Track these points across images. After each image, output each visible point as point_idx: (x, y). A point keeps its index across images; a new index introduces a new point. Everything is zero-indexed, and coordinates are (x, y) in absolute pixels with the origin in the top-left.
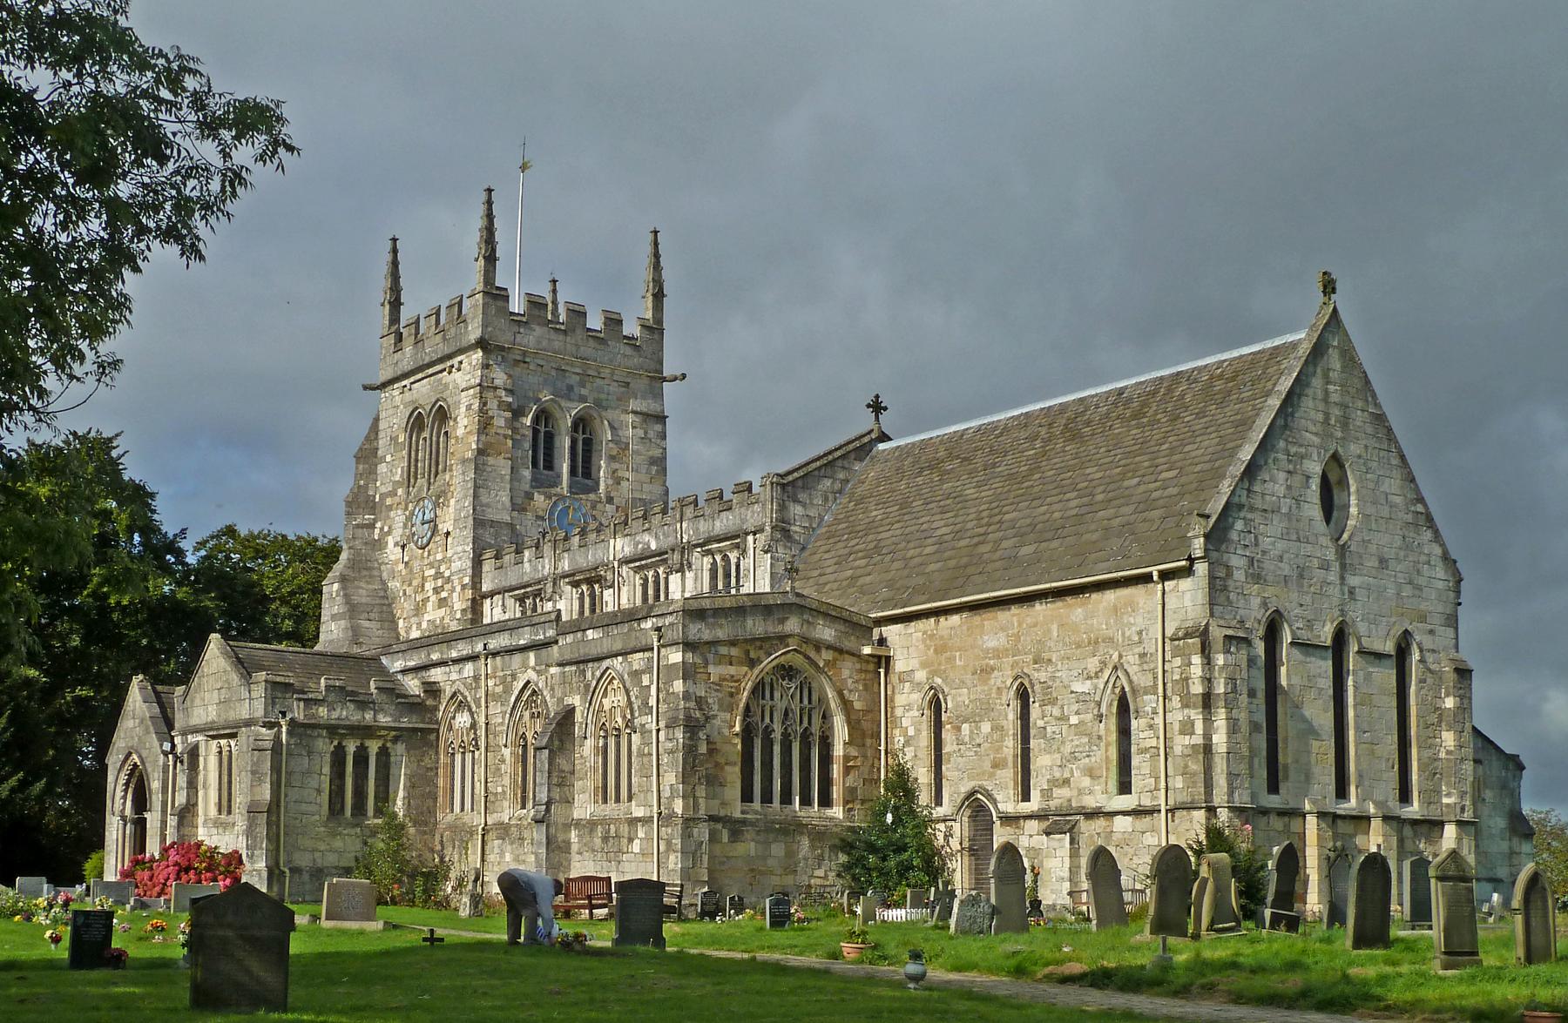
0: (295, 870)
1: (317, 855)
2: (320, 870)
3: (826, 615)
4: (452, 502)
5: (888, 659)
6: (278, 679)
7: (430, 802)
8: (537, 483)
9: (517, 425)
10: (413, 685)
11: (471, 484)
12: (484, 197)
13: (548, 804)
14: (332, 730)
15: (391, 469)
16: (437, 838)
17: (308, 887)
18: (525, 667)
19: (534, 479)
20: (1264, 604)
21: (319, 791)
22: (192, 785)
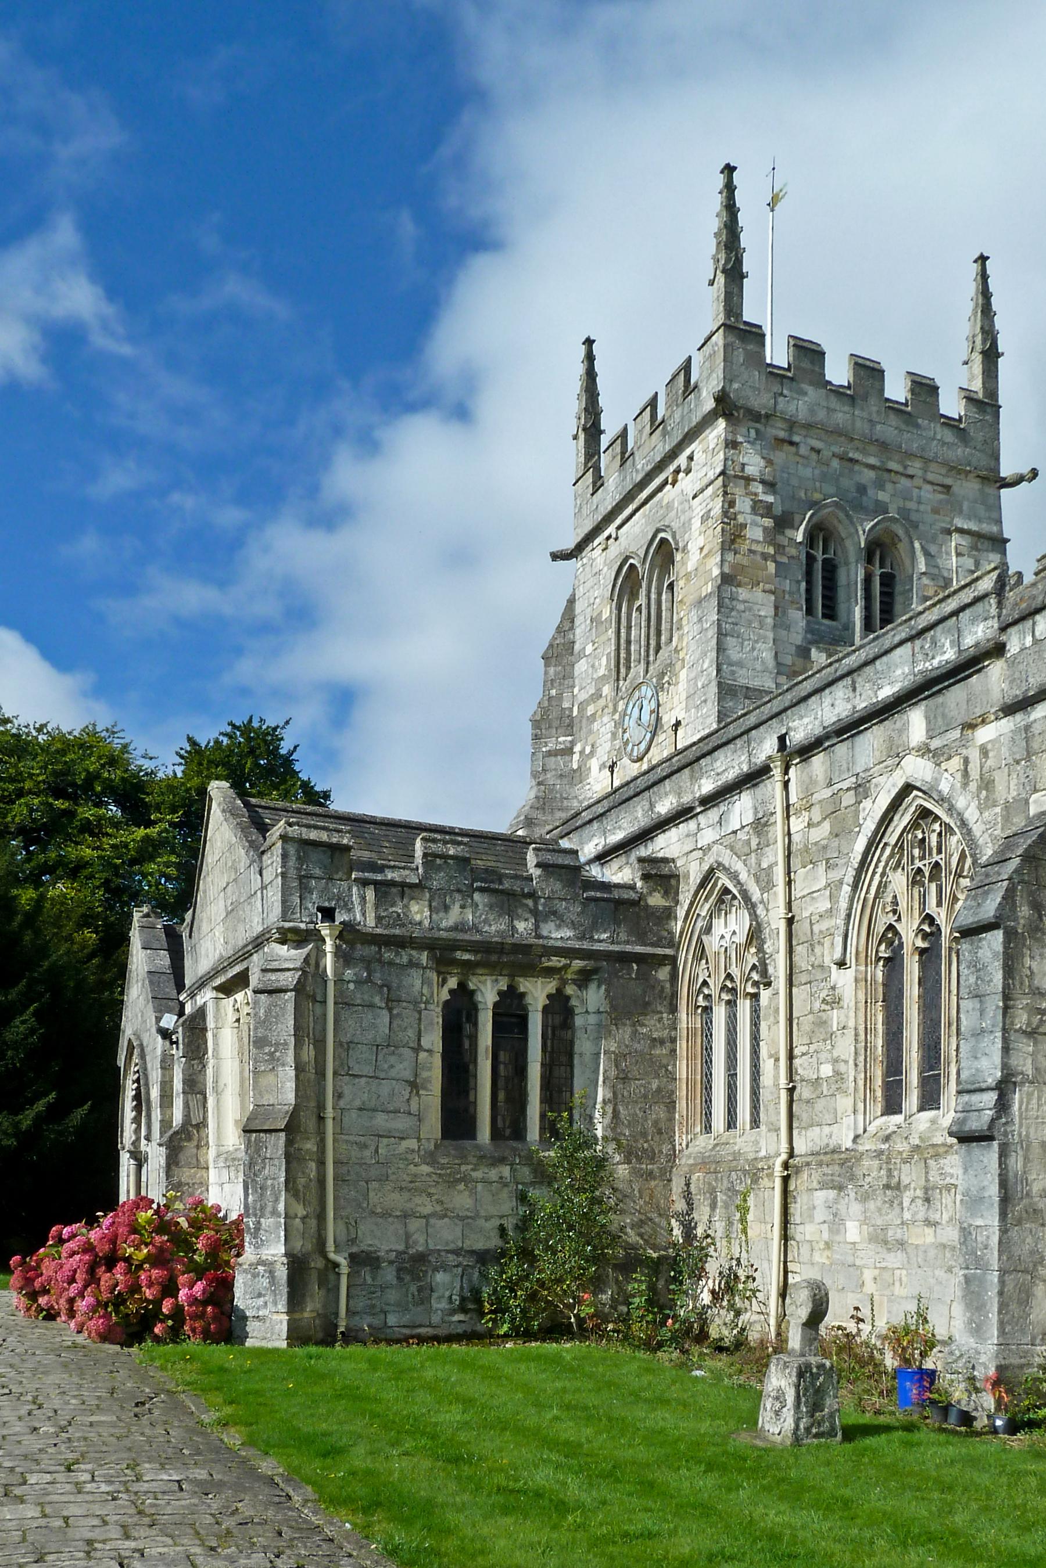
0: (362, 1260)
1: (414, 1225)
2: (421, 1258)
4: (683, 675)
6: (313, 835)
7: (660, 1112)
8: (816, 638)
9: (782, 540)
10: (621, 873)
11: (712, 632)
12: (720, 180)
13: (1005, 1087)
14: (443, 953)
15: (593, 660)
16: (677, 1186)
17: (392, 1296)
18: (896, 754)
19: (809, 630)
21: (415, 1086)
22: (194, 1086)
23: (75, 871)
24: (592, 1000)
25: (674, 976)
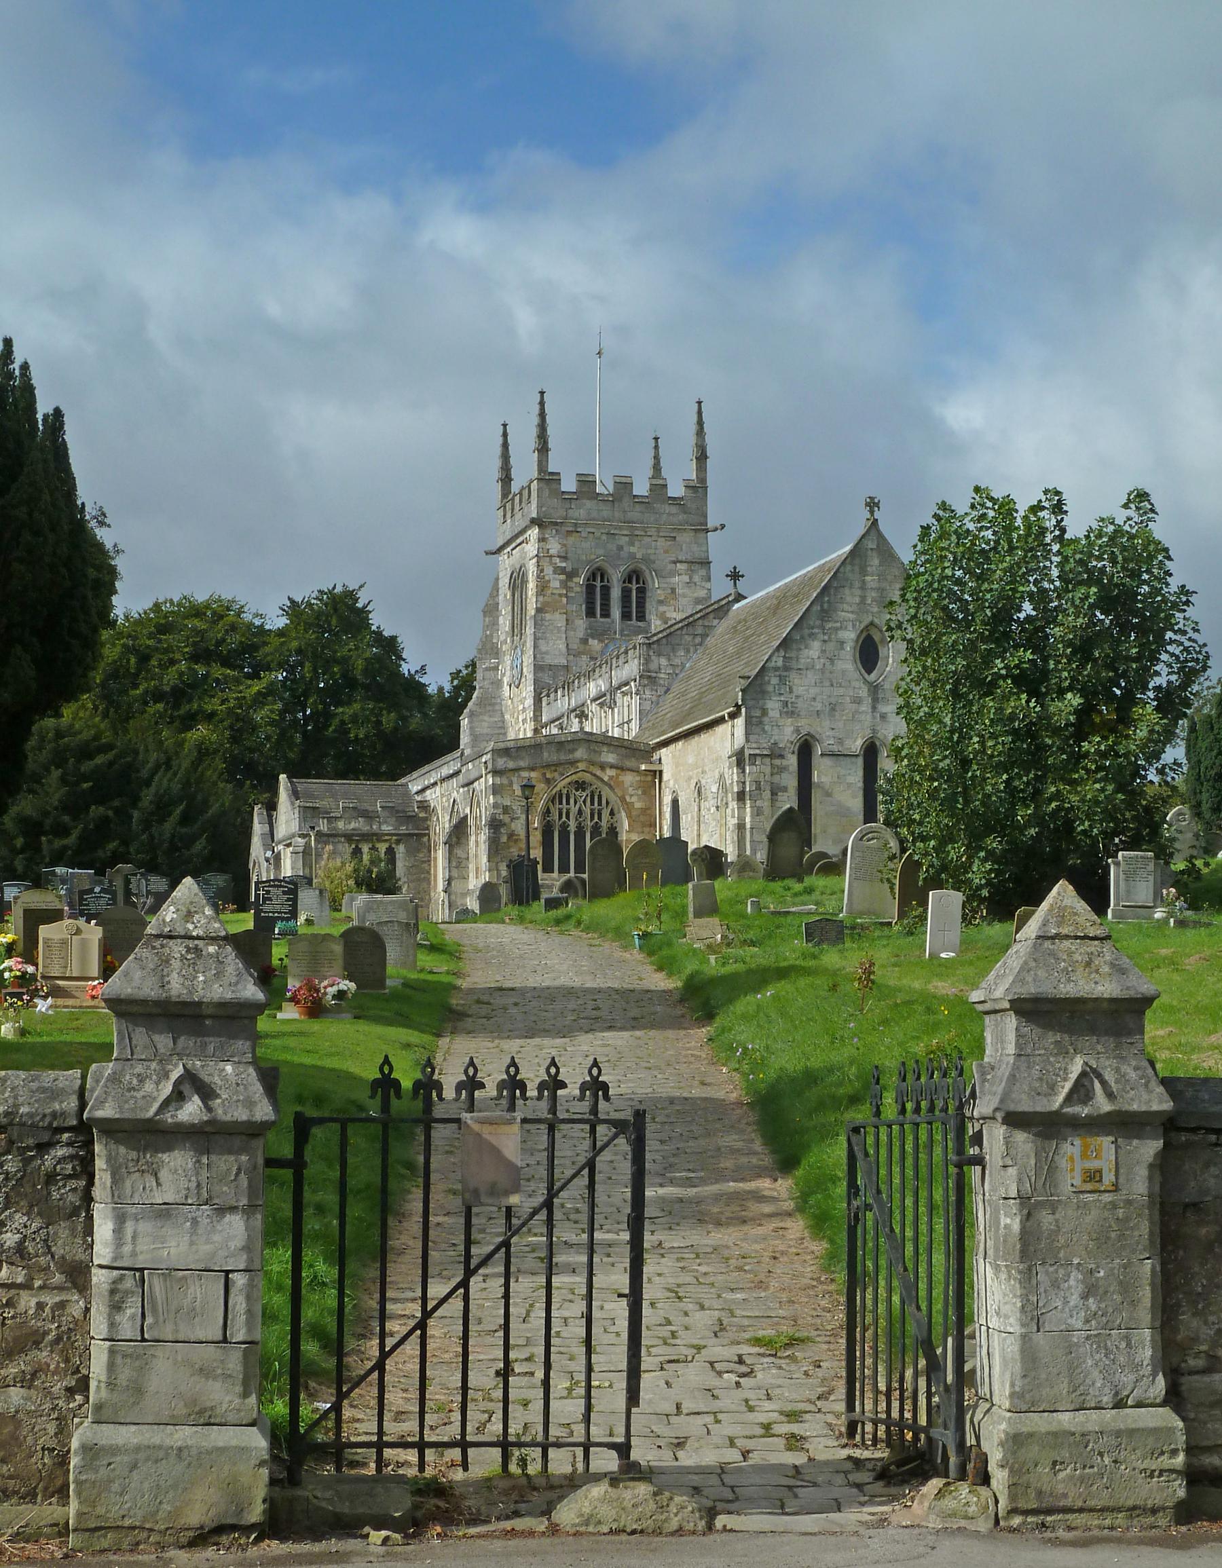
3: (609, 745)
5: (661, 772)
8: (594, 633)
14: (349, 837)
20: (797, 731)
23: (210, 717)
24: (401, 850)
25: (429, 840)
